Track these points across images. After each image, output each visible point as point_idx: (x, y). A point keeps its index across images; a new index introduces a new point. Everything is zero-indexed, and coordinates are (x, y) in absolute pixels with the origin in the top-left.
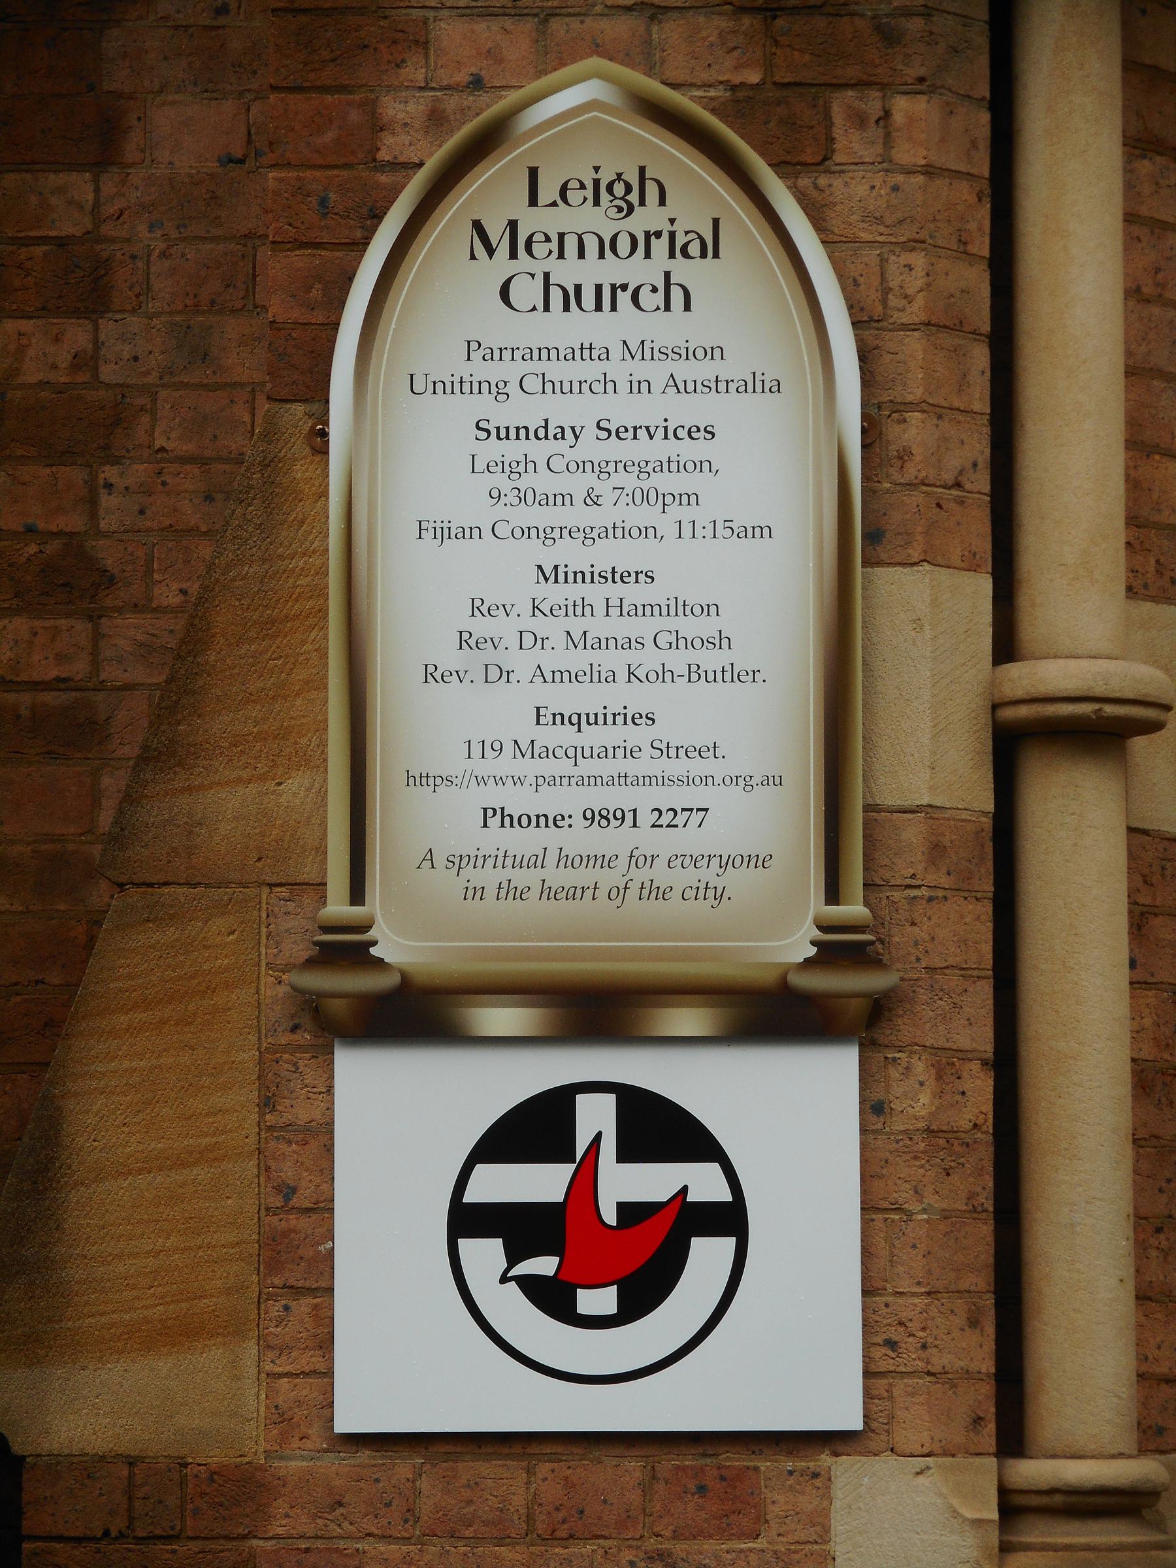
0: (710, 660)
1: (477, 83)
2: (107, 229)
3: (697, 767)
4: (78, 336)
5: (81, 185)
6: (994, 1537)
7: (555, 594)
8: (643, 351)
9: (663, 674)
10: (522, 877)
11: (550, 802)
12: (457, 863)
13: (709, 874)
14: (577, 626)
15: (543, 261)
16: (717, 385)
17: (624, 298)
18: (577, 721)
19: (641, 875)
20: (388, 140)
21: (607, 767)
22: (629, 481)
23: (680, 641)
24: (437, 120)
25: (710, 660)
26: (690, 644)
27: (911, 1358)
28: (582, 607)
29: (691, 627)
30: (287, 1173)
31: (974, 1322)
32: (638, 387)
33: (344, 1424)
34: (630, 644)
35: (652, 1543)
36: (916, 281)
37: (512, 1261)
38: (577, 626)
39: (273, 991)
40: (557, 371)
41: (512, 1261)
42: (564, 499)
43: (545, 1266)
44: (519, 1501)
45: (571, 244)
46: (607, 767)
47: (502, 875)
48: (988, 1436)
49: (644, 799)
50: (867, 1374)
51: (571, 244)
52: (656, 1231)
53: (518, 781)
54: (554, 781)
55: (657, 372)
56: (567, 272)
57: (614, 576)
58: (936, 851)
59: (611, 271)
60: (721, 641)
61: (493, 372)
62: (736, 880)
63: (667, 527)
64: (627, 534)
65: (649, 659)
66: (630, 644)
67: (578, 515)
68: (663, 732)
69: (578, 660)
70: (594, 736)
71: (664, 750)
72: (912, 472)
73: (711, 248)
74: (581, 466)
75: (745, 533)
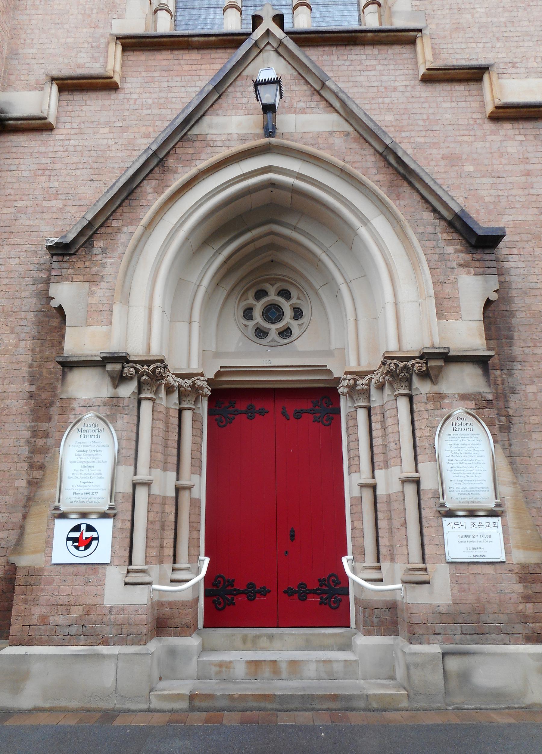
0: (99, 476)
1: (80, 414)
2: (49, 429)
3: (97, 488)
4: (45, 440)
5: (47, 424)
6: (125, 575)
7: (83, 469)
8: (94, 442)
9: (94, 478)
10: (77, 500)
11: (81, 492)
12: (70, 499)
13: (97, 500)
14: (85, 472)
15: (85, 433)
16: (102, 446)
17: (93, 436)
18: (84, 483)
19: (90, 500)
20: (70, 420)
21: (87, 488)
22: (92, 456)
23: (96, 474)
24: (75, 418)
25: (99, 476)
26: (97, 474)
27: (116, 554)
28: (86, 470)
29: (98, 472)
30: (49, 534)
31: (125, 550)
32: (94, 446)
33: (53, 562)
34: (90, 474)
35: (86, 576)
36: (125, 434)
37: (73, 543)
38: (85, 472)
39: (49, 513)
40: (85, 444)
41: (73, 543)
42: (84, 458)
43: (76, 544)
44: (72, 571)
45: (88, 431)
46: (87, 488)
47: (75, 500)
48: (127, 563)
49: (91, 491)
50: (111, 556)
51: (88, 431)
52: (89, 540)
53: (78, 489)
54: (81, 489)
55: (96, 445)
56: (87, 434)
57: (90, 467)
58: (123, 497)
59: (92, 434)
60: (101, 474)
61: (78, 445)
62: (100, 500)
63: (96, 461)
64: (91, 462)
65: (93, 476)
66: (90, 474)
67: (87, 460)
68: (93, 484)
69: (85, 476)
70: (86, 484)
71: (93, 486)
72: (123, 455)
73: (103, 431)
74: (87, 455)
75: (104, 462)
